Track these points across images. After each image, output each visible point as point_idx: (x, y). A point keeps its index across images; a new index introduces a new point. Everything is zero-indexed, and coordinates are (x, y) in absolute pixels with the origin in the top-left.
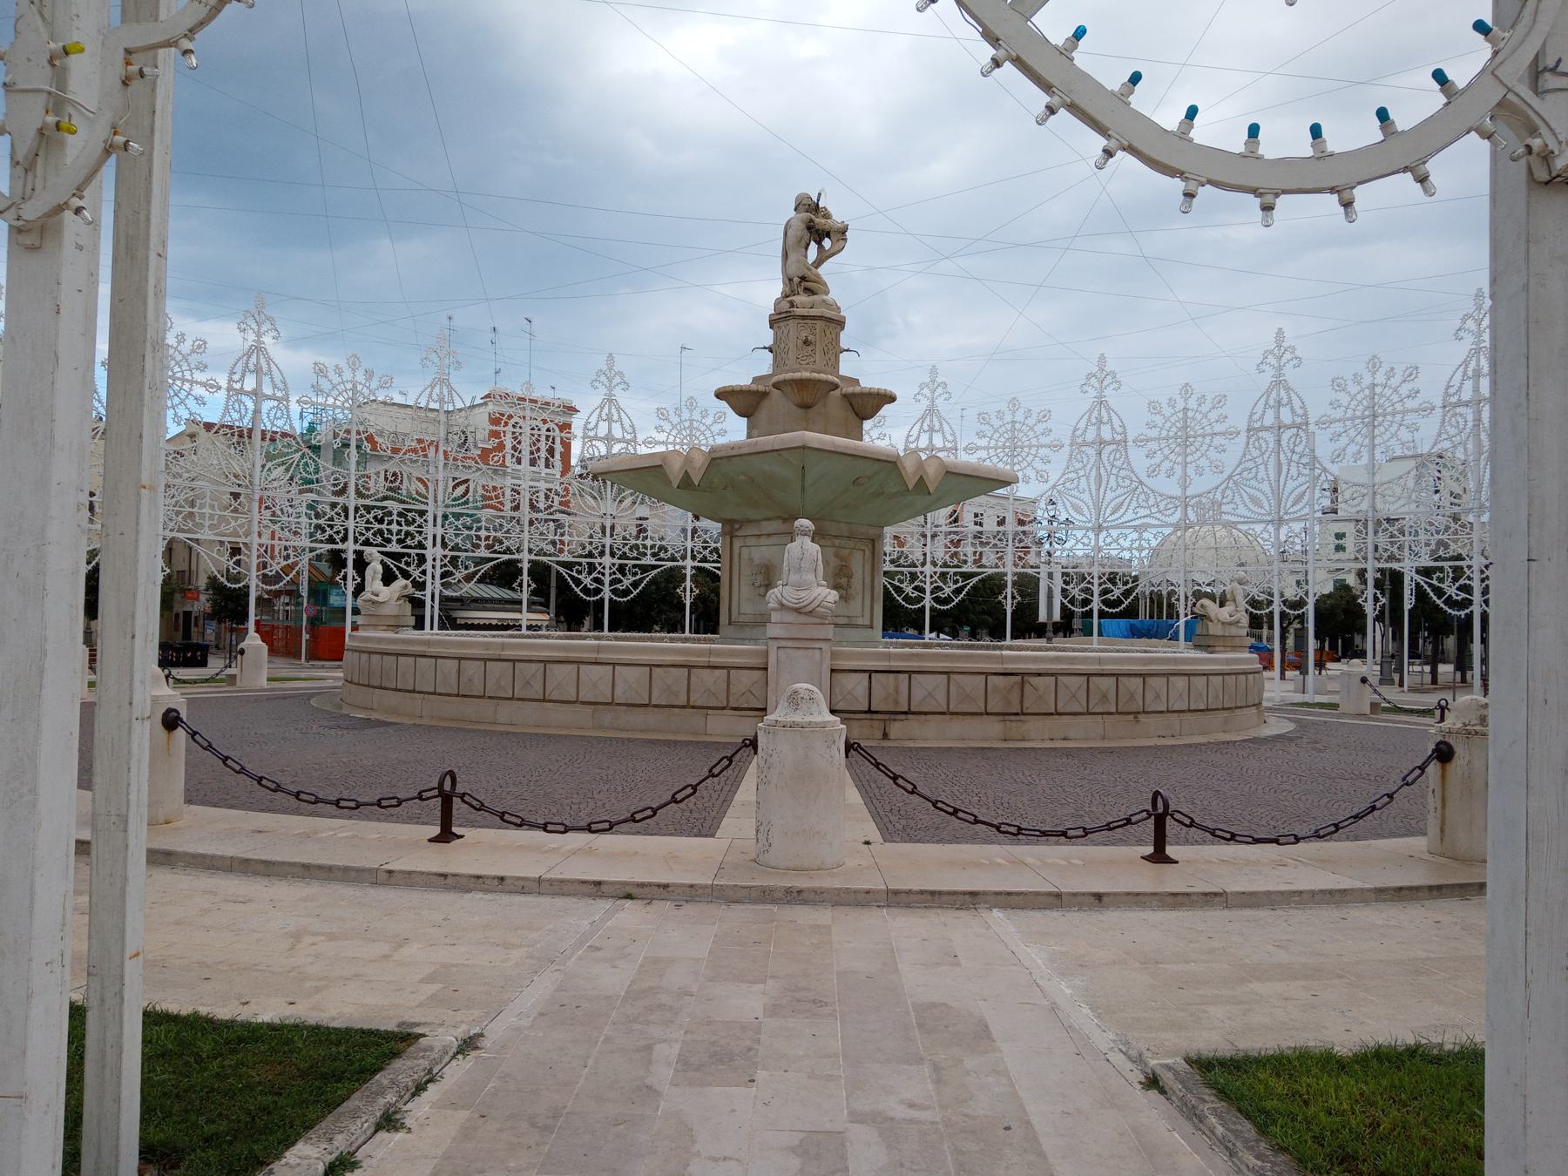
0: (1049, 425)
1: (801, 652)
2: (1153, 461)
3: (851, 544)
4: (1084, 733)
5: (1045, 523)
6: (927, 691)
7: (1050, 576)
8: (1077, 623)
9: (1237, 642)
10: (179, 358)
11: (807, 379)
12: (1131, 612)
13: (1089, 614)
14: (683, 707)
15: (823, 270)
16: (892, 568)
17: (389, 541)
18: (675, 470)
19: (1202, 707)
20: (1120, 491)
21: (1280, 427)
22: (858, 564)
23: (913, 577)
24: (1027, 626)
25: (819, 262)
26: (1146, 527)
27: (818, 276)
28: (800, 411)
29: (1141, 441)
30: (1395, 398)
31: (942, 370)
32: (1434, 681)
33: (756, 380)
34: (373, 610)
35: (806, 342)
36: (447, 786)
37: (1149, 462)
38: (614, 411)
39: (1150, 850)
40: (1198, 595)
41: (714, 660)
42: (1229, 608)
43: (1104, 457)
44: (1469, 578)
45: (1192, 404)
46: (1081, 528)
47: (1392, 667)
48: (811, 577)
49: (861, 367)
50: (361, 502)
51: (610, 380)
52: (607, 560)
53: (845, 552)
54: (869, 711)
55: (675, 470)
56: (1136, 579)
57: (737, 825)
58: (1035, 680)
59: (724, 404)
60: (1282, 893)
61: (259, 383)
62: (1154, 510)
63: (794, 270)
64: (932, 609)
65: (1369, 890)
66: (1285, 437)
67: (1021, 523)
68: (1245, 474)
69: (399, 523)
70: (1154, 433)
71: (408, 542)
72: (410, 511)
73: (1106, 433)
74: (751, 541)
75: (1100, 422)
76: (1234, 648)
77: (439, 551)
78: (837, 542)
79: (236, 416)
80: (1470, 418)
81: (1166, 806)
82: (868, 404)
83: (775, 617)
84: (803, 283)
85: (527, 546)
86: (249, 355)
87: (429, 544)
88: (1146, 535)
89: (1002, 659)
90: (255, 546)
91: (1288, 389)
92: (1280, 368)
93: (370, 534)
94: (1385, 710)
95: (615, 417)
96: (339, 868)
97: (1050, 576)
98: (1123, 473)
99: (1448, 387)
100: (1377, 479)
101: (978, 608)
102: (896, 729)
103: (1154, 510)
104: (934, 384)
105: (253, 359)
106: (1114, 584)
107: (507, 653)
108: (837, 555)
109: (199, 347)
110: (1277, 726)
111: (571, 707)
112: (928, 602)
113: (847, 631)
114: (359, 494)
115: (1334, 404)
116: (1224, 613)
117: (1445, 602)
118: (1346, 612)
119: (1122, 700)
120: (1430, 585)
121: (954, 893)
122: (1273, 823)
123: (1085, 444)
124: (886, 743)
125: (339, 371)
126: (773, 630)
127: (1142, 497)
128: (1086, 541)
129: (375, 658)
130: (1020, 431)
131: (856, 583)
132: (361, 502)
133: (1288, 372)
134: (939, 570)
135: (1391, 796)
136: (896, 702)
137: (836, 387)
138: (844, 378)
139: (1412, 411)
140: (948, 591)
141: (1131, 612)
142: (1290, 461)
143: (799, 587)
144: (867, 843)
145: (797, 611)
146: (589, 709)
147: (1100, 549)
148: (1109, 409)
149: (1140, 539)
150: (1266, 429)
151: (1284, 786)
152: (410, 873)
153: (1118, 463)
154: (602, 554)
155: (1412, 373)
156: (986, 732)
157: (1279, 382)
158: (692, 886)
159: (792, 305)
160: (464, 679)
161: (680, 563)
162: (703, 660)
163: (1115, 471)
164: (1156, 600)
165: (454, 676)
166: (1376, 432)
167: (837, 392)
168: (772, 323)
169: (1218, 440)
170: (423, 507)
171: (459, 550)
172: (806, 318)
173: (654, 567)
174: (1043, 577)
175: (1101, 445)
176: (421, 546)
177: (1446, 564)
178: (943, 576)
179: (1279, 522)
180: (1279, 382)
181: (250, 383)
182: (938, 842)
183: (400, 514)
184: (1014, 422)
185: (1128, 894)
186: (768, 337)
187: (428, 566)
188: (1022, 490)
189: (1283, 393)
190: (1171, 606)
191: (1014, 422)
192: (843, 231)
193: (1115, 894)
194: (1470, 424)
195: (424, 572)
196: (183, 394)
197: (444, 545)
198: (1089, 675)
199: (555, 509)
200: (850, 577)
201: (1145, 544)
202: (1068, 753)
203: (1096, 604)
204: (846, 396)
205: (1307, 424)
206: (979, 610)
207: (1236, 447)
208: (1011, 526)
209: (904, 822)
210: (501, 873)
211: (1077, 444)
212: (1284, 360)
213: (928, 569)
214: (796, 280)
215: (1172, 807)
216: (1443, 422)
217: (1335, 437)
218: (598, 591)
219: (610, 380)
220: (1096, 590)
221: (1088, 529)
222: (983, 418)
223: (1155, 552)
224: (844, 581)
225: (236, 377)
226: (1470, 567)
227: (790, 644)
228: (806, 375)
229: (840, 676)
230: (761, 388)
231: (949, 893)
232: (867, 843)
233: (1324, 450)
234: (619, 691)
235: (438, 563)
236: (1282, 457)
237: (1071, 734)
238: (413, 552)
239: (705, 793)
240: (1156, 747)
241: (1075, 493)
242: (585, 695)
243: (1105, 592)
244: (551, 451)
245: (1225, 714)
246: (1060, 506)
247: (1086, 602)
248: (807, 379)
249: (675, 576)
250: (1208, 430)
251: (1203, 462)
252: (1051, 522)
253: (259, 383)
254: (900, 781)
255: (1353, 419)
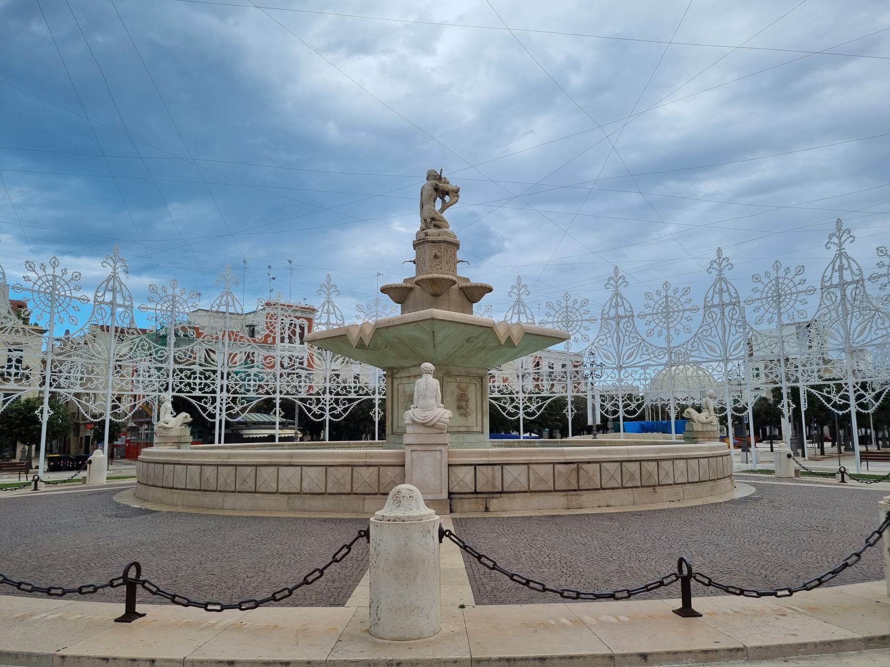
0: (587, 308)
1: (427, 453)
2: (650, 327)
3: (468, 380)
4: (620, 502)
5: (588, 366)
6: (515, 477)
7: (593, 397)
8: (610, 425)
9: (712, 435)
10: (62, 283)
11: (437, 280)
12: (641, 417)
13: (618, 419)
14: (349, 494)
15: (446, 215)
16: (499, 395)
17: (194, 389)
18: (354, 335)
19: (697, 480)
20: (631, 345)
21: (722, 305)
22: (473, 393)
23: (512, 400)
24: (581, 427)
25: (443, 210)
26: (648, 366)
27: (442, 217)
28: (433, 298)
29: (642, 316)
30: (791, 285)
31: (521, 268)
32: (823, 453)
33: (405, 281)
34: (164, 433)
35: (436, 257)
36: (132, 574)
37: (647, 328)
38: (331, 308)
39: (678, 603)
40: (683, 408)
41: (369, 461)
42: (704, 414)
43: (621, 325)
44: (846, 391)
45: (670, 293)
46: (609, 368)
47: (798, 443)
48: (433, 401)
49: (470, 273)
50: (177, 366)
51: (328, 289)
52: (328, 396)
53: (464, 386)
54: (475, 492)
55: (354, 335)
56: (643, 398)
57: (361, 594)
58: (585, 466)
59: (386, 297)
60: (790, 646)
61: (114, 298)
62: (652, 356)
63: (427, 215)
64: (524, 419)
65: (859, 640)
66: (727, 310)
67: (575, 366)
68: (704, 333)
69: (200, 378)
70: (649, 311)
71: (206, 390)
72: (207, 371)
73: (621, 312)
74: (405, 381)
75: (617, 305)
76: (710, 439)
77: (225, 394)
78: (458, 379)
79: (99, 317)
80: (839, 294)
81: (690, 569)
82: (473, 294)
83: (409, 430)
84: (432, 222)
85: (281, 388)
86: (108, 280)
87: (218, 390)
88: (648, 371)
89: (563, 453)
90: (110, 395)
91: (726, 283)
92: (720, 271)
93: (182, 386)
94: (803, 474)
95: (332, 311)
96: (23, 654)
97: (593, 397)
98: (632, 335)
99: (823, 277)
100: (784, 334)
101: (553, 418)
102: (494, 504)
103: (652, 356)
104: (519, 285)
105: (111, 283)
106: (631, 401)
107: (232, 461)
108: (458, 387)
109: (76, 276)
110: (743, 491)
111: (274, 497)
112: (521, 415)
113: (467, 436)
114: (176, 362)
115: (755, 290)
116: (702, 417)
117: (833, 406)
118: (766, 413)
119: (644, 479)
120: (822, 396)
121: (527, 659)
122: (763, 571)
123: (609, 318)
124: (487, 515)
125: (164, 289)
126: (407, 439)
127: (645, 348)
128: (613, 375)
129: (151, 465)
130: (571, 312)
131: (472, 404)
132: (177, 366)
133: (726, 273)
134: (527, 395)
135: (858, 555)
136: (493, 485)
137: (455, 283)
138: (459, 278)
139: (802, 292)
140: (533, 408)
141: (641, 417)
142: (730, 325)
143: (425, 408)
144: (462, 607)
145: (424, 425)
146: (285, 498)
147: (622, 381)
148: (622, 298)
149: (645, 373)
150: (715, 306)
151: (763, 538)
152: (79, 657)
153: (629, 329)
154: (324, 393)
155: (801, 269)
156: (554, 505)
157: (721, 278)
158: (309, 663)
159: (426, 235)
160: (204, 478)
161: (372, 397)
162: (361, 461)
163: (628, 334)
164: (654, 409)
165: (198, 475)
166: (781, 305)
167: (455, 287)
168: (415, 246)
169: (687, 314)
170: (214, 368)
171: (238, 393)
172: (434, 242)
173: (548, 398)
174: (589, 398)
175: (618, 319)
176: (214, 392)
177: (831, 383)
178: (530, 399)
179: (727, 361)
180: (721, 278)
181: (108, 297)
182: (517, 602)
183: (201, 373)
184: (567, 307)
185: (668, 653)
186: (412, 254)
187: (217, 404)
188: (575, 346)
189: (723, 285)
190: (663, 412)
191: (567, 307)
192: (456, 192)
193: (658, 654)
194: (839, 298)
195: (215, 408)
196: (65, 305)
197: (228, 391)
198: (621, 462)
199: (292, 368)
200: (467, 401)
201: (648, 376)
202: (611, 517)
203: (621, 414)
204: (461, 289)
205: (739, 302)
206: (553, 420)
207: (698, 317)
208: (570, 368)
209: (492, 584)
210: (152, 656)
211: (605, 318)
212: (723, 265)
213: (521, 395)
214: (429, 220)
215: (694, 569)
216: (822, 298)
217: (757, 309)
218: (322, 415)
219: (328, 289)
220: (621, 405)
221: (614, 369)
222: (549, 305)
223: (654, 381)
224: (464, 403)
225: (99, 294)
226: (846, 384)
227: (419, 448)
228: (435, 275)
229: (454, 469)
230: (409, 285)
231: (522, 659)
232: (462, 607)
233: (751, 317)
234: (305, 484)
235: (224, 402)
236: (726, 322)
237: (612, 503)
238: (209, 395)
239: (349, 563)
240: (669, 510)
241: (605, 347)
242: (283, 488)
243: (625, 406)
244: (294, 332)
245: (711, 484)
246: (596, 355)
247: (615, 412)
248: (437, 280)
249: (370, 404)
250: (681, 308)
251: (679, 327)
252: (592, 365)
253: (114, 298)
254: (483, 559)
255: (767, 298)
